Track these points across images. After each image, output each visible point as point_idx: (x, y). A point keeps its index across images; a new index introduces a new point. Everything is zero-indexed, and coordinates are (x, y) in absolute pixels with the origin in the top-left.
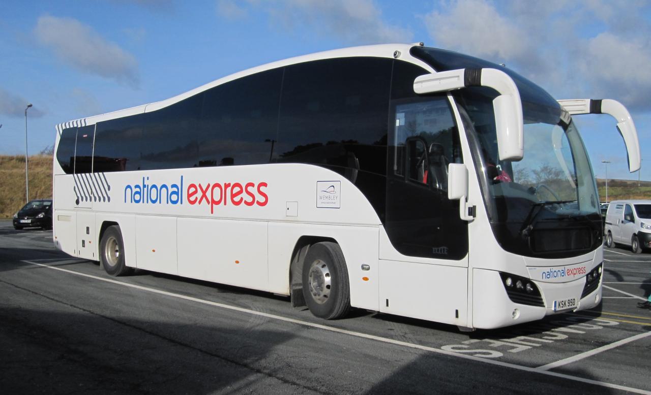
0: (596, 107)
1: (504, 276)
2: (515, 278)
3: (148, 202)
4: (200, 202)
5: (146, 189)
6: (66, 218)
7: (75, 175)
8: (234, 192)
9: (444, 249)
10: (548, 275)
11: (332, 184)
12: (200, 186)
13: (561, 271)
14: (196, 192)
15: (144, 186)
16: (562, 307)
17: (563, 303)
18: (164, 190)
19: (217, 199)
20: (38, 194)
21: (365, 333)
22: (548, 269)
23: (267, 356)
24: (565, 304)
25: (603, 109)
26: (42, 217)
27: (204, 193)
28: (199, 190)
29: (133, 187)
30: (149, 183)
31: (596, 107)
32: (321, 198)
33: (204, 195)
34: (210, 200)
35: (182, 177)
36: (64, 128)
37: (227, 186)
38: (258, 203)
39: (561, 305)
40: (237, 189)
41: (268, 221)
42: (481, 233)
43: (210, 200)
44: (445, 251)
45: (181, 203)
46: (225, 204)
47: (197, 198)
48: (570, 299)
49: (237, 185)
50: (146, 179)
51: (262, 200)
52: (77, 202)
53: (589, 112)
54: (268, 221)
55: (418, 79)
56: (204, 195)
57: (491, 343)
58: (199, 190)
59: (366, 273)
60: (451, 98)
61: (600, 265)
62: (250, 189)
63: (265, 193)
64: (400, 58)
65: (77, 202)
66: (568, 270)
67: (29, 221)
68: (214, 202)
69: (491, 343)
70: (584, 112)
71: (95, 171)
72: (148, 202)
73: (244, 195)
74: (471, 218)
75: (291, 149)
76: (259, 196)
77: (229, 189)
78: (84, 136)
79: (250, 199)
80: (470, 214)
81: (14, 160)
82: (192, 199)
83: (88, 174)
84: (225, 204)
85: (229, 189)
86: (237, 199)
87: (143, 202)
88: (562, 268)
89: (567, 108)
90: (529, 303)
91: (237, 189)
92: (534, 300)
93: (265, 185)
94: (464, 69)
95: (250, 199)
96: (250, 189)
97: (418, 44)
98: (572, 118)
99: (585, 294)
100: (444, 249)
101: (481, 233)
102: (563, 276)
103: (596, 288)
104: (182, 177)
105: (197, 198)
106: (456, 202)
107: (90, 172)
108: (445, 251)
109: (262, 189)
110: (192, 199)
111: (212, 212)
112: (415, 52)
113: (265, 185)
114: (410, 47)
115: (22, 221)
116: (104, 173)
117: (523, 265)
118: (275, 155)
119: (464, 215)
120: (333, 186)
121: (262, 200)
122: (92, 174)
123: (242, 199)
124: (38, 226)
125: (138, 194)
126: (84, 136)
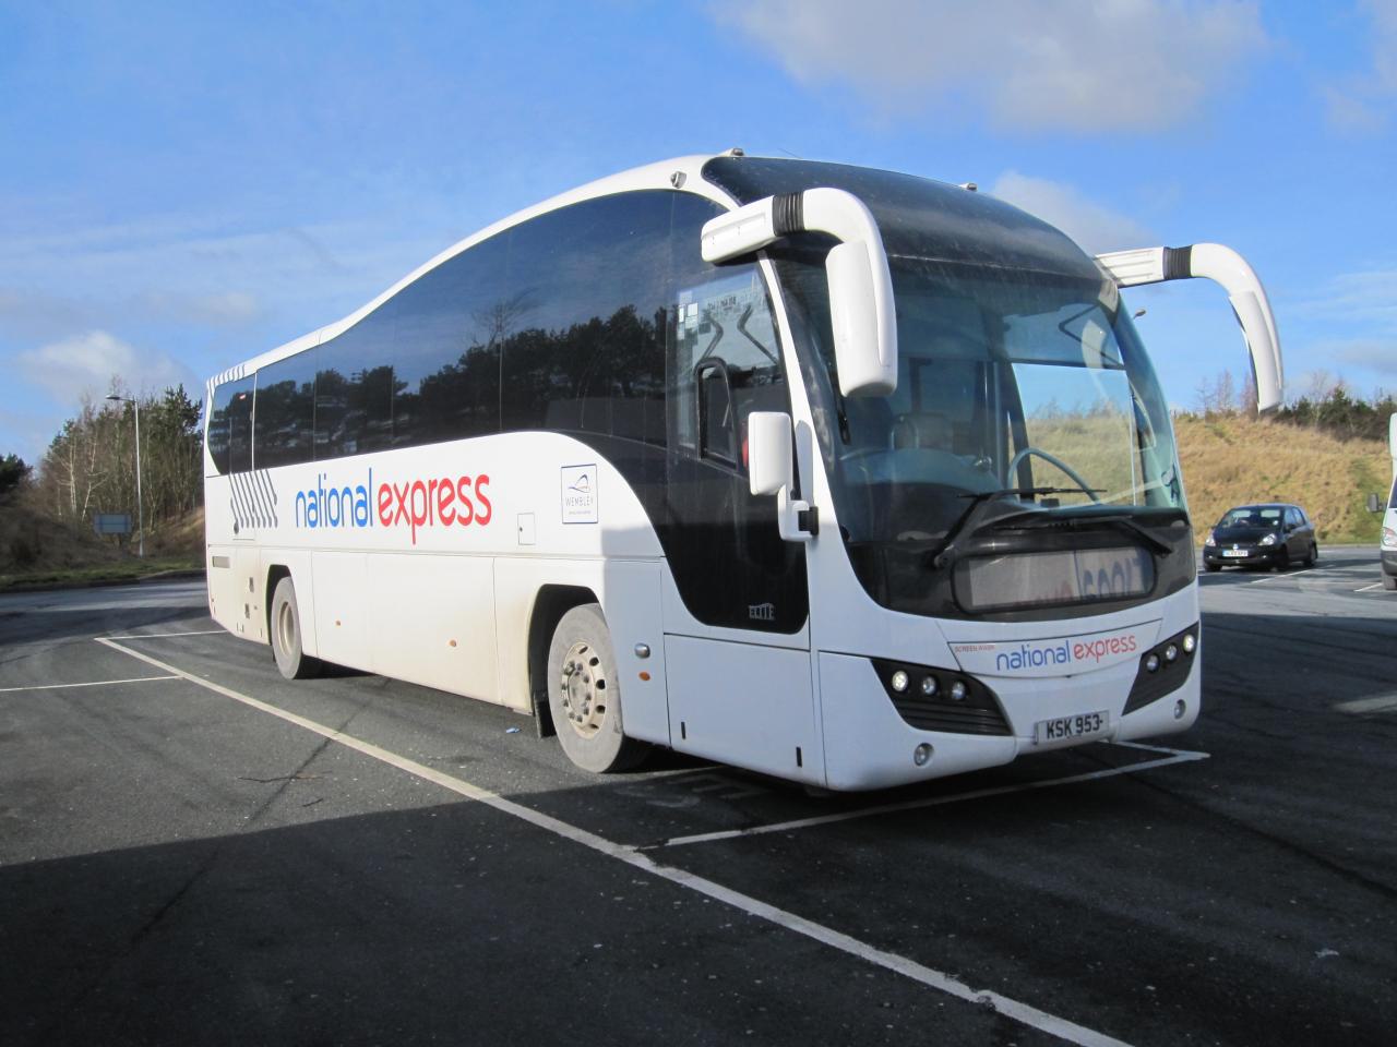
0: (1178, 264)
1: (885, 668)
2: (916, 672)
3: (264, 525)
5: (1027, 655)
6: (222, 562)
7: (231, 475)
8: (443, 499)
9: (768, 609)
10: (1017, 660)
11: (583, 471)
13: (1008, 655)
14: (389, 501)
15: (1024, 652)
16: (1058, 735)
17: (1062, 726)
18: (347, 497)
19: (1100, 651)
20: (1048, 496)
22: (1017, 648)
24: (1067, 727)
25: (1197, 265)
26: (1271, 543)
27: (1090, 650)
29: (354, 491)
30: (327, 486)
31: (1178, 264)
32: (568, 503)
36: (217, 384)
37: (433, 484)
39: (1056, 732)
40: (1115, 643)
42: (830, 571)
44: (771, 612)
45: (372, 524)
47: (392, 513)
48: (1082, 712)
49: (1115, 640)
50: (322, 477)
51: (1132, 646)
52: (236, 530)
53: (1162, 277)
55: (708, 227)
59: (645, 665)
60: (766, 265)
61: (1191, 630)
63: (488, 498)
64: (684, 188)
65: (236, 530)
66: (385, 488)
67: (1245, 553)
68: (1098, 654)
70: (1151, 279)
71: (256, 468)
73: (1121, 646)
74: (806, 535)
76: (455, 502)
79: (1124, 648)
80: (802, 528)
81: (1059, 431)
82: (386, 514)
83: (247, 473)
85: (435, 491)
86: (447, 512)
88: (1061, 643)
89: (1116, 272)
90: (962, 727)
91: (1115, 643)
92: (971, 720)
93: (1133, 637)
94: (771, 198)
95: (1124, 648)
97: (727, 154)
98: (1123, 297)
99: (1133, 704)
100: (768, 609)
101: (830, 571)
102: (1062, 662)
103: (1179, 687)
105: (392, 513)
106: (769, 500)
107: (249, 469)
108: (771, 612)
111: (414, 542)
112: (714, 171)
114: (703, 160)
115: (1227, 554)
116: (270, 470)
117: (925, 639)
119: (788, 530)
120: (585, 476)
121: (1132, 646)
122: (253, 473)
125: (316, 506)
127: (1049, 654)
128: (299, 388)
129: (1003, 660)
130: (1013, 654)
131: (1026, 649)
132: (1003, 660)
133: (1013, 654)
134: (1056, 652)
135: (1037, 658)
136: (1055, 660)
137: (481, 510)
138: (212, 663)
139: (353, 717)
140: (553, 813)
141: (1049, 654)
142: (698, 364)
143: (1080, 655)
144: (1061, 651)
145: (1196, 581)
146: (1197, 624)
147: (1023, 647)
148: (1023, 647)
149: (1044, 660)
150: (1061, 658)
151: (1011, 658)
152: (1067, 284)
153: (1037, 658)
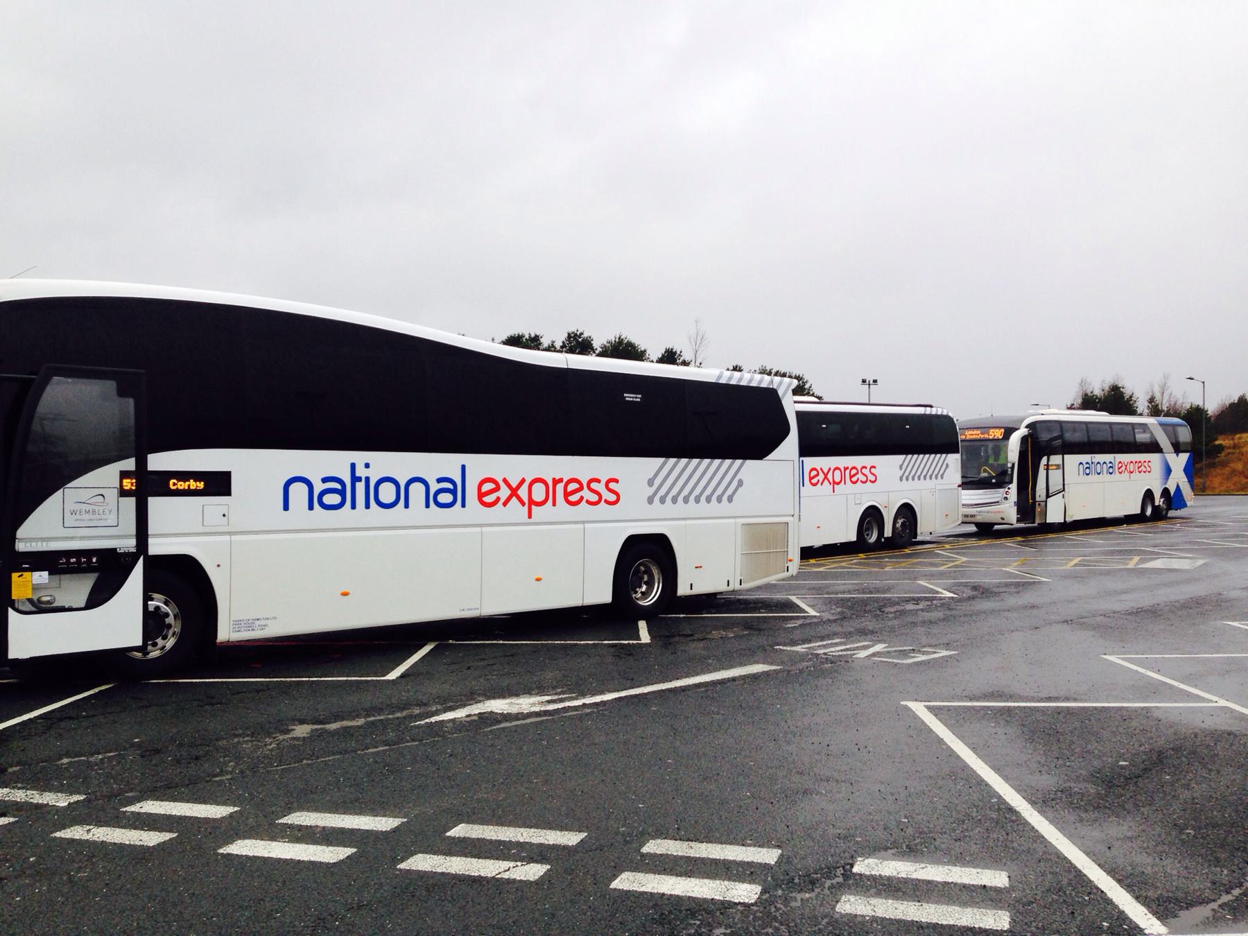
3: (367, 506)
4: (505, 504)
5: (360, 487)
12: (505, 480)
15: (355, 479)
19: (837, 480)
21: (744, 678)
23: (1171, 731)
27: (826, 476)
28: (502, 485)
33: (826, 477)
34: (526, 499)
37: (846, 469)
38: (606, 502)
40: (854, 472)
41: (583, 522)
43: (526, 499)
45: (463, 505)
46: (554, 504)
49: (854, 468)
51: (613, 498)
54: (583, 522)
56: (826, 477)
58: (502, 485)
62: (593, 485)
68: (532, 502)
72: (367, 506)
73: (860, 476)
76: (852, 475)
77: (560, 487)
78: (629, 397)
79: (594, 498)
84: (554, 504)
85: (560, 487)
87: (353, 507)
91: (854, 472)
93: (616, 481)
95: (594, 498)
96: (593, 485)
105: (498, 499)
109: (612, 485)
110: (814, 481)
111: (463, 467)
113: (616, 481)
121: (613, 498)
123: (582, 498)
124: (563, 693)
126: (629, 397)
129: (299, 491)
130: (439, 480)
132: (299, 491)
133: (439, 480)
135: (387, 493)
136: (431, 499)
137: (871, 477)
141: (417, 490)
143: (489, 499)
145: (791, 443)
147: (353, 466)
148: (353, 466)
150: (445, 498)
151: (434, 487)
153: (387, 493)
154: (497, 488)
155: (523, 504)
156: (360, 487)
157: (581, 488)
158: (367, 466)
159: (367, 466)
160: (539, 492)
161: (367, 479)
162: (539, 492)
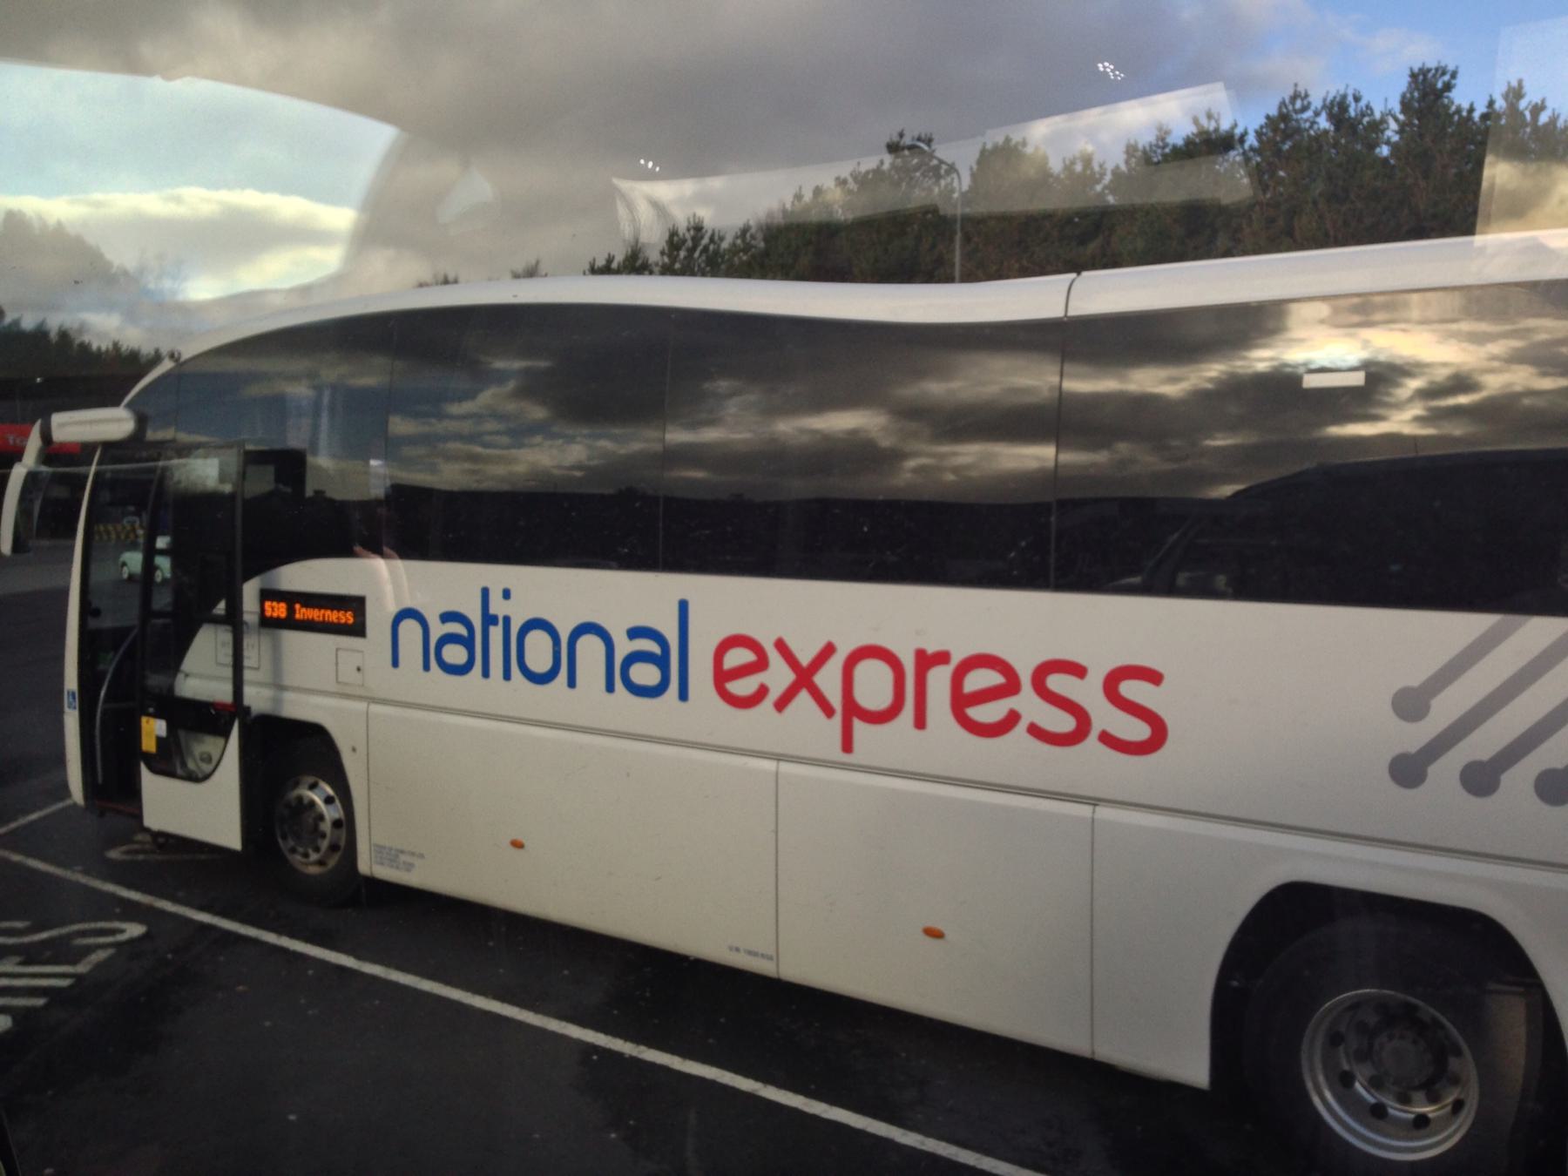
3: (507, 676)
4: (781, 704)
5: (496, 633)
12: (781, 646)
15: (489, 620)
27: (804, 678)
28: (774, 657)
35: (395, 663)
37: (925, 661)
41: (1095, 802)
43: (836, 700)
46: (920, 722)
51: (1139, 731)
54: (1095, 802)
57: (955, 454)
58: (774, 657)
68: (852, 711)
69: (955, 454)
72: (507, 676)
73: (1028, 704)
75: (1432, 770)
77: (939, 680)
79: (1063, 723)
84: (920, 722)
85: (939, 680)
87: (486, 673)
95: (1063, 723)
104: (395, 663)
105: (762, 692)
113: (1154, 677)
118: (1182, 579)
123: (1012, 719)
127: (410, 628)
128: (1123, 167)
129: (410, 628)
131: (498, 607)
133: (634, 633)
134: (438, 630)
135: (539, 651)
138: (1454, 327)
139: (221, 447)
140: (180, 894)
141: (590, 647)
142: (623, 196)
144: (457, 628)
146: (128, 630)
147: (485, 593)
148: (485, 593)
149: (564, 666)
152: (956, 171)
153: (539, 651)
154: (761, 664)
155: (828, 710)
156: (496, 633)
157: (1011, 686)
158: (507, 594)
159: (507, 594)
160: (873, 685)
161: (507, 620)
162: (873, 685)
